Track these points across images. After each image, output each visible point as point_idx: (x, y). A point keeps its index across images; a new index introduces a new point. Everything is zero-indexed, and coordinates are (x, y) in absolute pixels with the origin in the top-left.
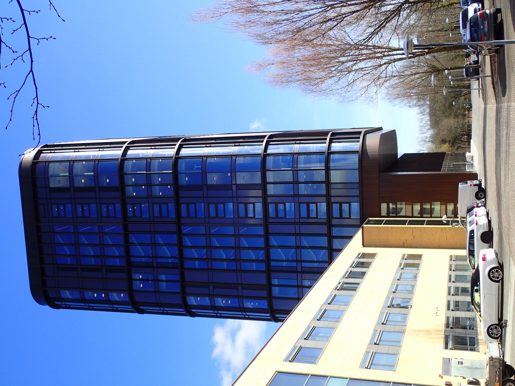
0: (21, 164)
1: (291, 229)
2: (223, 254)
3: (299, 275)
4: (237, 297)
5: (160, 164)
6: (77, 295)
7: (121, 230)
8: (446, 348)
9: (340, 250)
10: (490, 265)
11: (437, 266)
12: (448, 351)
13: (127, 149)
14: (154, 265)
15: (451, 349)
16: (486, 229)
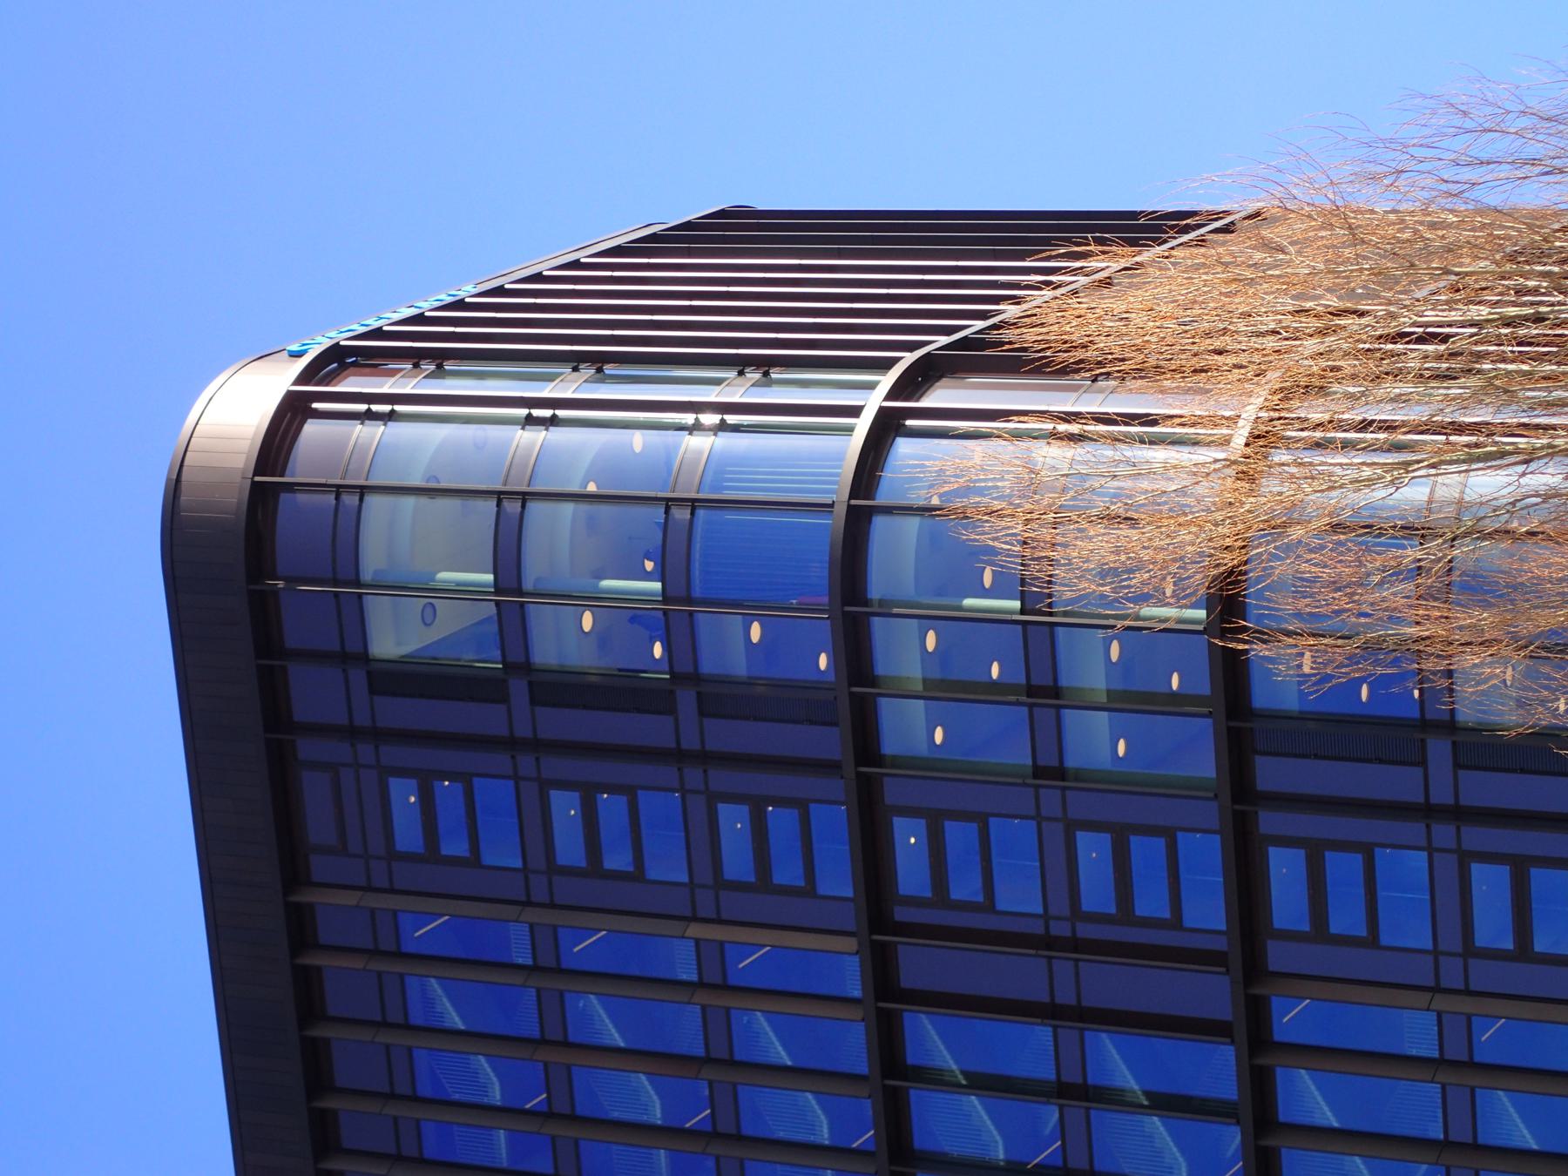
0: (175, 488)
1: (1022, 975)
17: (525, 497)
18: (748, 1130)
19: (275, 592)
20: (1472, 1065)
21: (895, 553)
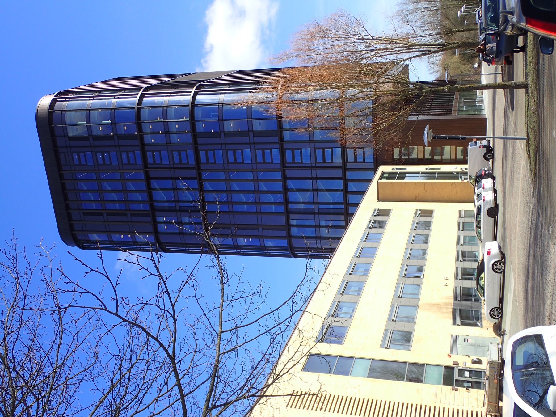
0: (37, 113)
1: (167, 173)
2: (243, 197)
3: (317, 216)
4: (258, 236)
5: (176, 111)
6: (104, 237)
7: (143, 176)
8: (454, 323)
9: (357, 205)
10: (494, 258)
11: (447, 218)
12: (456, 327)
13: (142, 96)
14: (178, 209)
15: (458, 325)
16: (492, 205)
17: (90, 110)
18: (130, 200)
19: (53, 127)
20: (230, 179)
21: (145, 113)
